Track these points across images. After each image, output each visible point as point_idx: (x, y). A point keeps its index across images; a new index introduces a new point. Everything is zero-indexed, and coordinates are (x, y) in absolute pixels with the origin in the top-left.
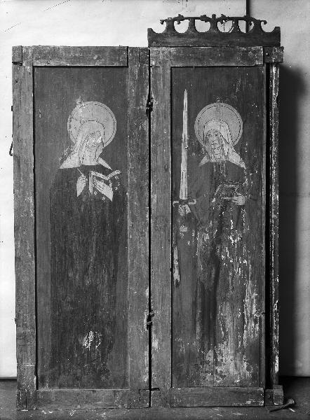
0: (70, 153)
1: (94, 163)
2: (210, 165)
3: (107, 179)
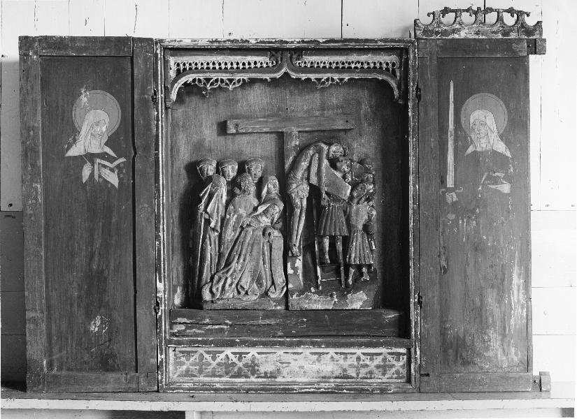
0: (75, 141)
1: (99, 151)
2: (475, 153)
3: (111, 166)
